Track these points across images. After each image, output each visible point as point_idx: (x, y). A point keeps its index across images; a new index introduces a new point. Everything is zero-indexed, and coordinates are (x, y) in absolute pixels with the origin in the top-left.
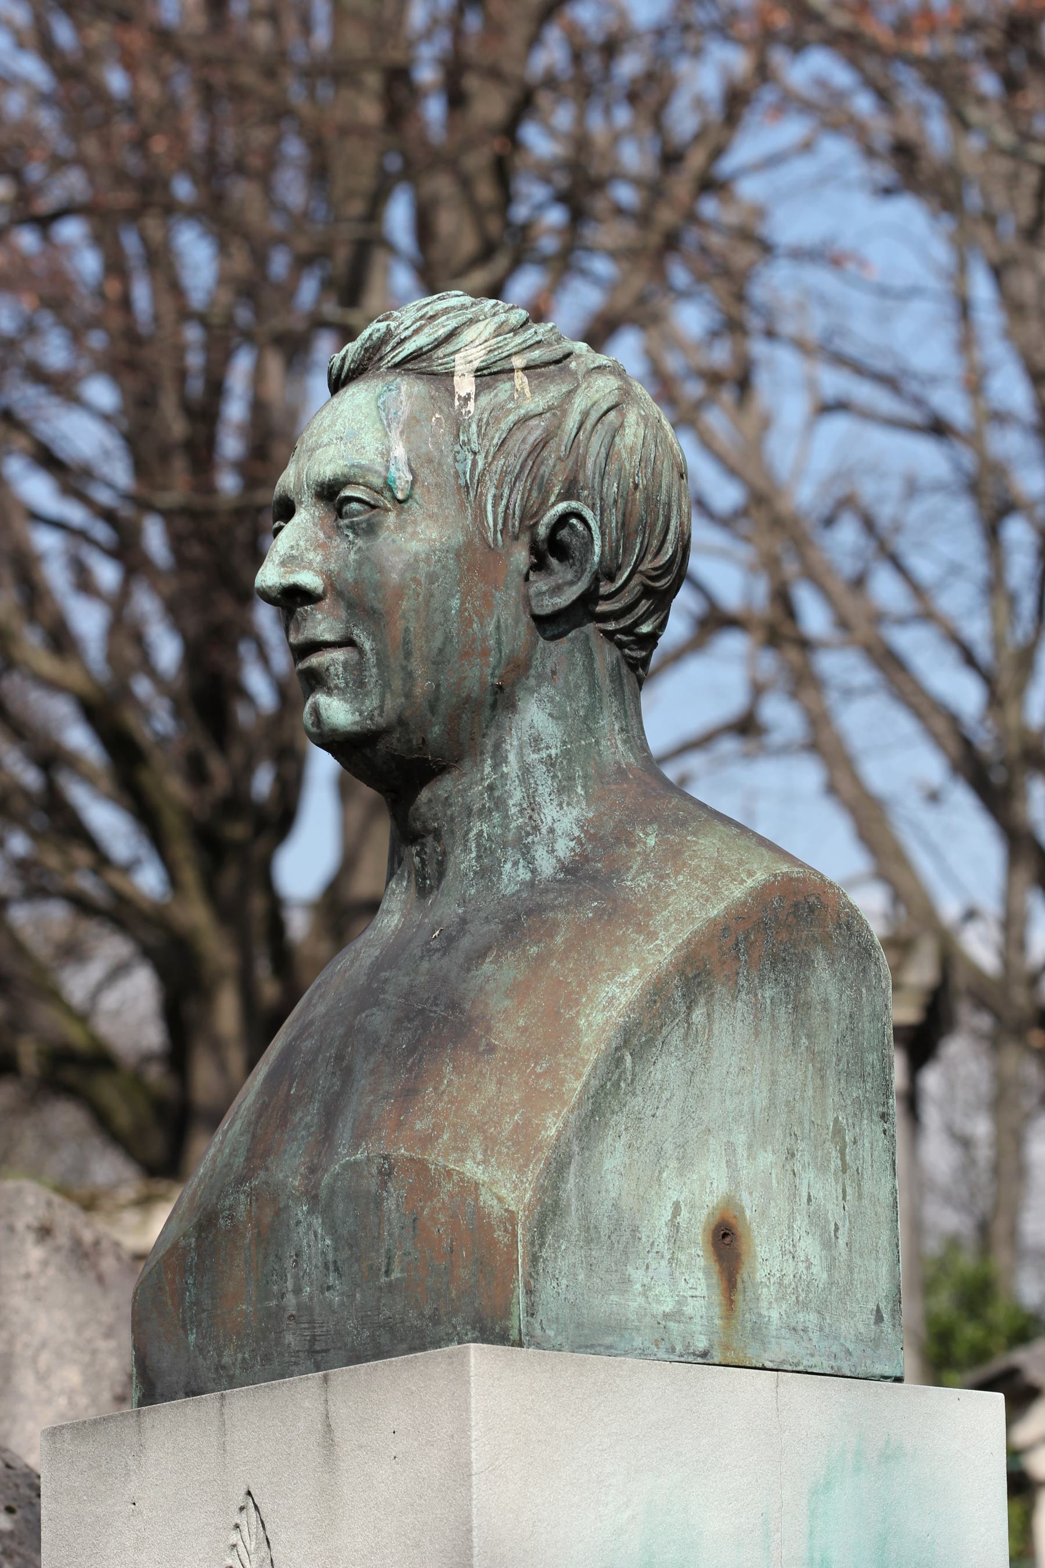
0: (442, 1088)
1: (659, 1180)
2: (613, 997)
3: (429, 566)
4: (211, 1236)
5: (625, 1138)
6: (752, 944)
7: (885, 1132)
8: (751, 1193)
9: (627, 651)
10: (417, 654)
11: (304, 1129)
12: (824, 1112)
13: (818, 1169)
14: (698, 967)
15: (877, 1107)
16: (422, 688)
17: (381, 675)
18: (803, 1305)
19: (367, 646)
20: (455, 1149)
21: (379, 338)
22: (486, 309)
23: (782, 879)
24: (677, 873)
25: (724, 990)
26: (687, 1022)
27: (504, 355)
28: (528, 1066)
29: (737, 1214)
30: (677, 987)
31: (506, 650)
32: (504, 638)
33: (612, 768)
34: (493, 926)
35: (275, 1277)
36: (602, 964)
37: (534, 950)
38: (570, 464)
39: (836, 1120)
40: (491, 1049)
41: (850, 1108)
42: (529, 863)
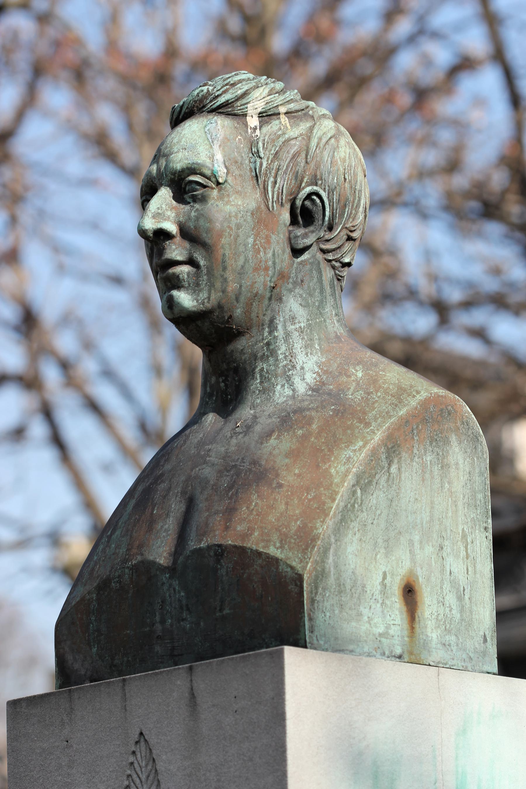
0: (252, 507)
1: (375, 559)
2: (350, 457)
3: (237, 219)
4: (106, 593)
5: (358, 536)
6: (420, 431)
7: (486, 537)
8: (422, 568)
9: (337, 272)
10: (230, 268)
11: (164, 532)
12: (457, 525)
13: (455, 557)
14: (393, 442)
15: (483, 523)
16: (232, 287)
17: (209, 280)
18: (448, 631)
19: (202, 263)
20: (263, 540)
21: (203, 95)
22: (262, 81)
23: (435, 396)
24: (377, 391)
25: (407, 456)
26: (388, 472)
27: (275, 105)
28: (303, 495)
29: (414, 579)
30: (383, 453)
31: (278, 267)
32: (277, 261)
33: (334, 335)
34: (274, 420)
35: (148, 615)
36: (341, 439)
37: (300, 432)
38: (313, 166)
39: (463, 530)
40: (280, 486)
41: (470, 523)
42: (290, 385)
